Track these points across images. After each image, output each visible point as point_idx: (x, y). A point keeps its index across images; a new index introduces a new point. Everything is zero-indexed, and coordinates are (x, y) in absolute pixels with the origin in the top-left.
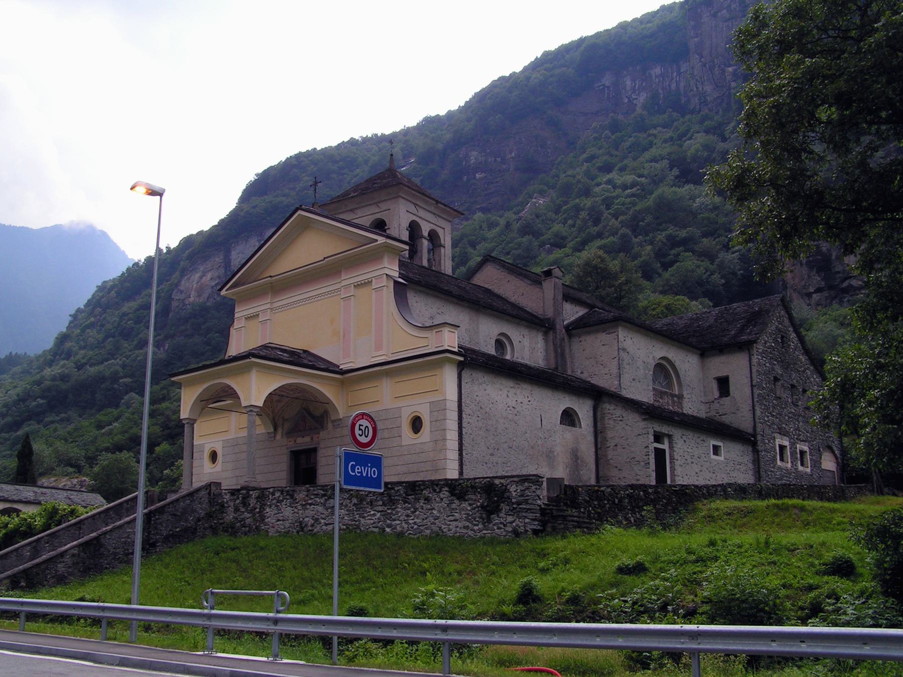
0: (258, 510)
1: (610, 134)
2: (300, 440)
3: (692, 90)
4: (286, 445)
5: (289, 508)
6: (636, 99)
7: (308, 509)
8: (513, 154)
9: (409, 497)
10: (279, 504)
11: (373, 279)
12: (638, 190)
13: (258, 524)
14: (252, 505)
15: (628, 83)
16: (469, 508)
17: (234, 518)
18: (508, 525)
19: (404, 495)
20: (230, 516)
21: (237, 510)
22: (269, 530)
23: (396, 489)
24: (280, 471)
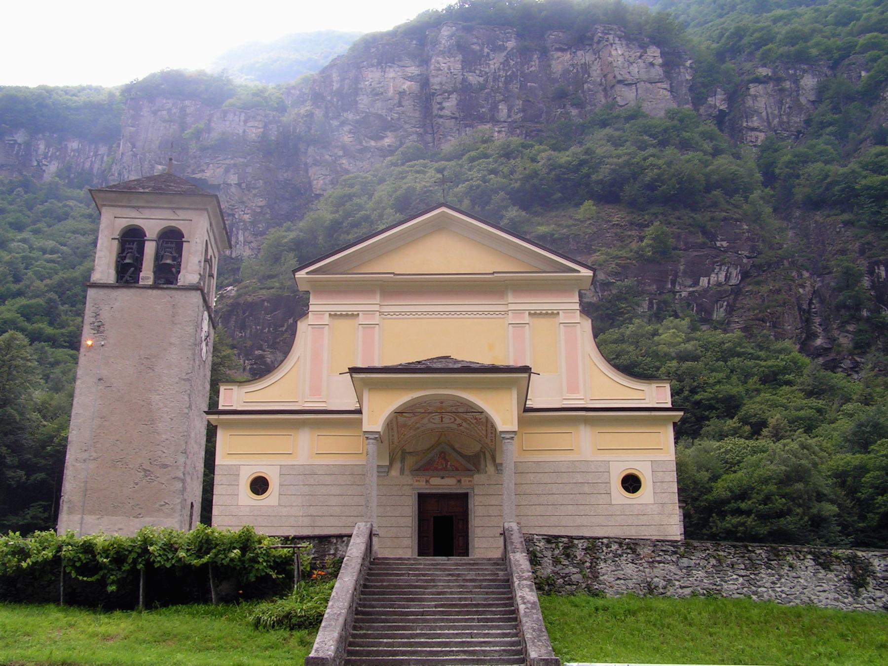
0: (588, 564)
2: (435, 481)
3: (113, 175)
4: (412, 485)
7: (656, 567)
9: (772, 562)
10: (617, 559)
11: (560, 312)
12: (59, 257)
13: (589, 582)
14: (579, 558)
15: (42, 147)
16: (836, 579)
17: (553, 572)
18: (878, 600)
19: (766, 560)
21: (556, 561)
22: (606, 591)
23: (758, 552)
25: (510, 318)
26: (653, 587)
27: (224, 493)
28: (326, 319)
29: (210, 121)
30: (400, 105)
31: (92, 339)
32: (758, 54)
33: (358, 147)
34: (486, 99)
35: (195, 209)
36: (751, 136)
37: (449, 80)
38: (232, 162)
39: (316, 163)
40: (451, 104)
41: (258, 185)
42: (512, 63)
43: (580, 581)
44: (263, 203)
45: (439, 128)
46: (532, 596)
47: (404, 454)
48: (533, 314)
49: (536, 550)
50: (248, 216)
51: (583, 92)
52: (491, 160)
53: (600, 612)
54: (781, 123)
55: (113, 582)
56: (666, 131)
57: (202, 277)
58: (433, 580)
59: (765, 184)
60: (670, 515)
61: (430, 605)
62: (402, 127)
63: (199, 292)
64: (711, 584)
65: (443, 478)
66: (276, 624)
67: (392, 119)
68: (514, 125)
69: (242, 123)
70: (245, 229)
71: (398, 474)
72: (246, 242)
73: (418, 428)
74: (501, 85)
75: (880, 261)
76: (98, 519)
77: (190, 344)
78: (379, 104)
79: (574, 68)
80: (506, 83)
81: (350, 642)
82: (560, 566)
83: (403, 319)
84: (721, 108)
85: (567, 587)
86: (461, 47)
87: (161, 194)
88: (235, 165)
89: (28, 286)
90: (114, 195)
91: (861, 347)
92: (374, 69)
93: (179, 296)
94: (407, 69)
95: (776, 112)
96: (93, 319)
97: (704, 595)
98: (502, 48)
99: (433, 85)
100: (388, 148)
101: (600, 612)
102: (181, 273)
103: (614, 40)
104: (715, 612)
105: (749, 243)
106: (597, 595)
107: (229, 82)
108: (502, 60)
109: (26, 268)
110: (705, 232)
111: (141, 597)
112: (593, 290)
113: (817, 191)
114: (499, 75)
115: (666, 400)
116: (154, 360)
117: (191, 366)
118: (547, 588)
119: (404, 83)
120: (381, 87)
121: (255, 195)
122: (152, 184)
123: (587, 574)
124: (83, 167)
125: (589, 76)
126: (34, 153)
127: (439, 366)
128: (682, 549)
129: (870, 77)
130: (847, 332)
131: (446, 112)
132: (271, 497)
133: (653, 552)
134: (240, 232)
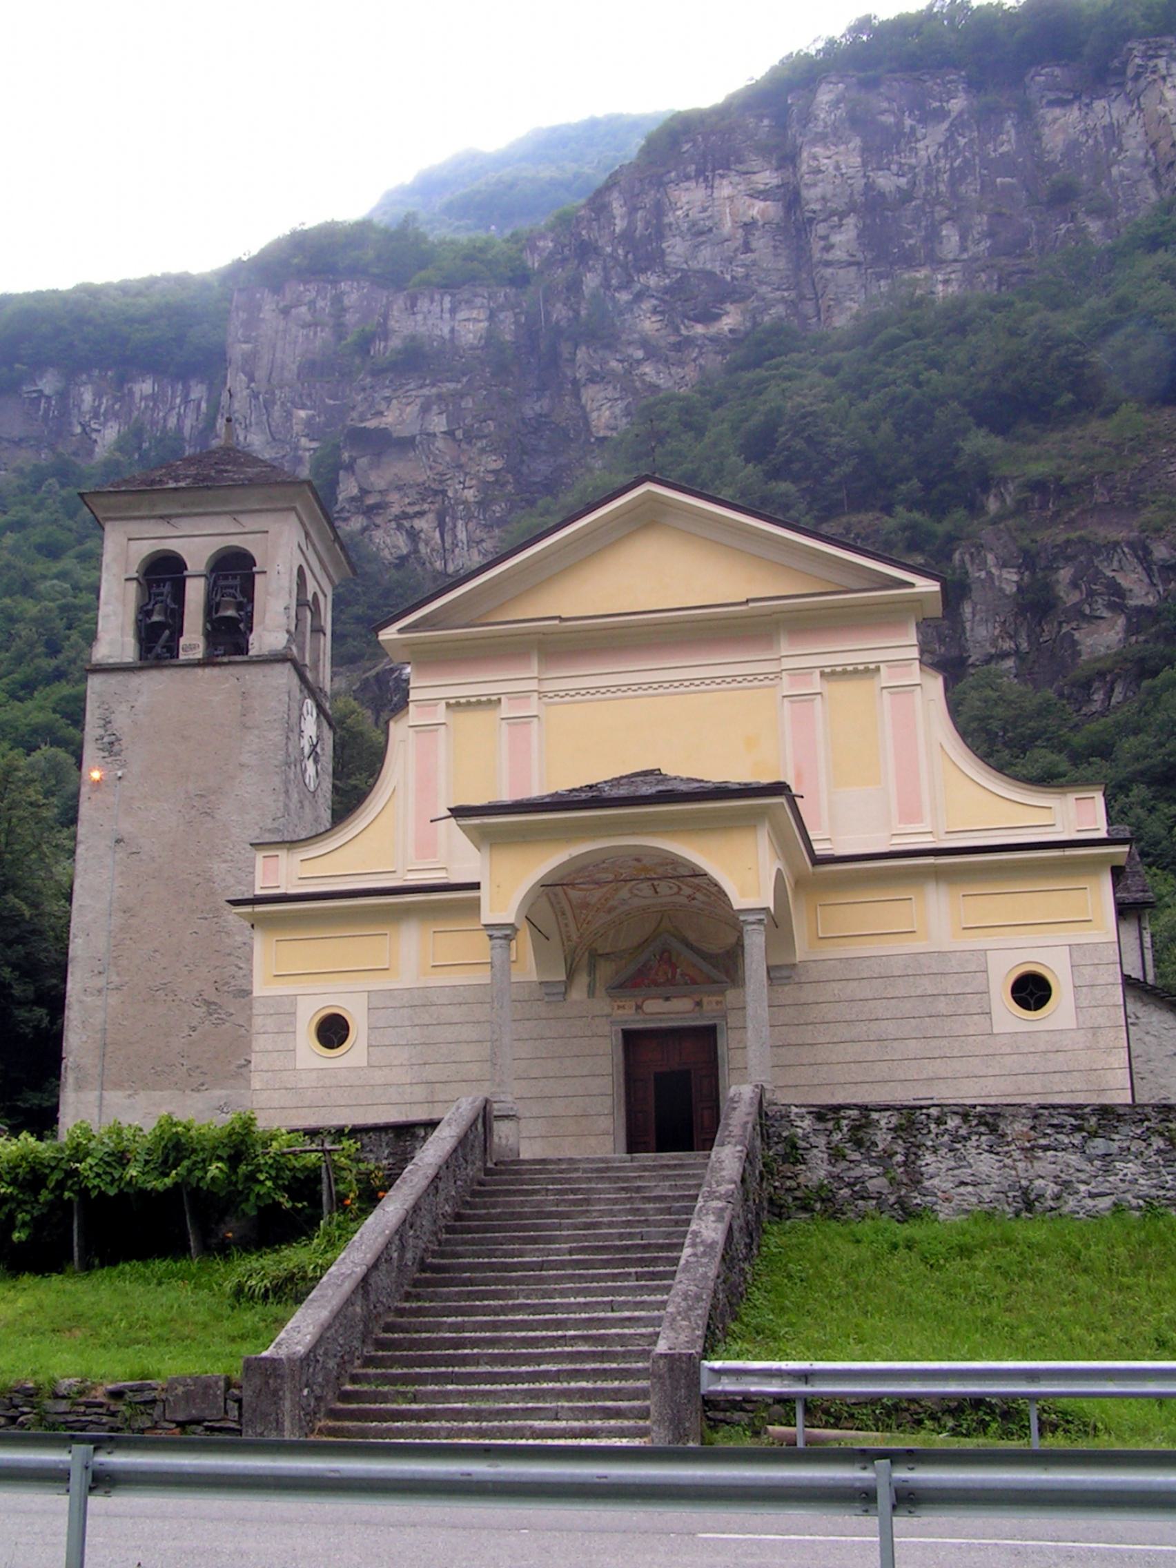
0: (899, 1158)
1: (57, 487)
2: (653, 1006)
4: (608, 1016)
5: (986, 1154)
6: (98, 431)
7: (1038, 1158)
10: (958, 1146)
11: (882, 666)
13: (903, 1192)
14: (881, 1146)
15: (88, 397)
17: (830, 1175)
20: (817, 1170)
21: (836, 1155)
22: (937, 1207)
24: (411, 1084)
25: (786, 686)
26: (1032, 1197)
27: (270, 1048)
28: (441, 714)
29: (386, 317)
30: (747, 248)
31: (100, 768)
33: (672, 339)
34: (915, 221)
35: (268, 510)
37: (838, 190)
38: (434, 390)
39: (594, 378)
40: (845, 238)
41: (486, 431)
42: (962, 141)
43: (885, 1191)
44: (499, 465)
45: (825, 287)
46: (715, 1230)
47: (595, 957)
48: (830, 675)
49: (796, 1135)
50: (472, 491)
51: (1110, 183)
52: (928, 340)
53: (902, 1251)
55: (24, 1224)
57: (295, 635)
58: (587, 1201)
60: (1109, 1050)
61: (560, 1251)
62: (754, 292)
63: (288, 665)
64: (1155, 1186)
65: (667, 999)
66: (271, 1293)
67: (733, 278)
68: (975, 266)
69: (447, 316)
70: (469, 518)
71: (585, 995)
72: (473, 542)
74: (942, 188)
76: (130, 1096)
77: (276, 763)
78: (706, 252)
79: (1089, 137)
80: (954, 183)
82: (844, 1164)
83: (605, 700)
85: (860, 1202)
86: (858, 121)
87: (208, 488)
88: (440, 397)
89: (72, 662)
90: (125, 498)
92: (692, 184)
93: (254, 677)
94: (755, 178)
96: (101, 732)
97: (1139, 1208)
98: (941, 114)
99: (807, 204)
100: (730, 336)
101: (902, 1251)
102: (254, 633)
104: (1146, 1244)
106: (919, 1216)
107: (420, 238)
108: (942, 139)
109: (69, 628)
111: (76, 1249)
112: (1147, 580)
114: (938, 170)
115: (1096, 823)
116: (213, 798)
117: (281, 805)
118: (818, 1206)
119: (750, 206)
120: (709, 218)
122: (192, 471)
123: (898, 1178)
124: (165, 427)
125: (1121, 149)
126: (76, 411)
127: (623, 791)
128: (1093, 1120)
131: (838, 254)
132: (354, 1052)
133: (1033, 1128)
134: (460, 523)
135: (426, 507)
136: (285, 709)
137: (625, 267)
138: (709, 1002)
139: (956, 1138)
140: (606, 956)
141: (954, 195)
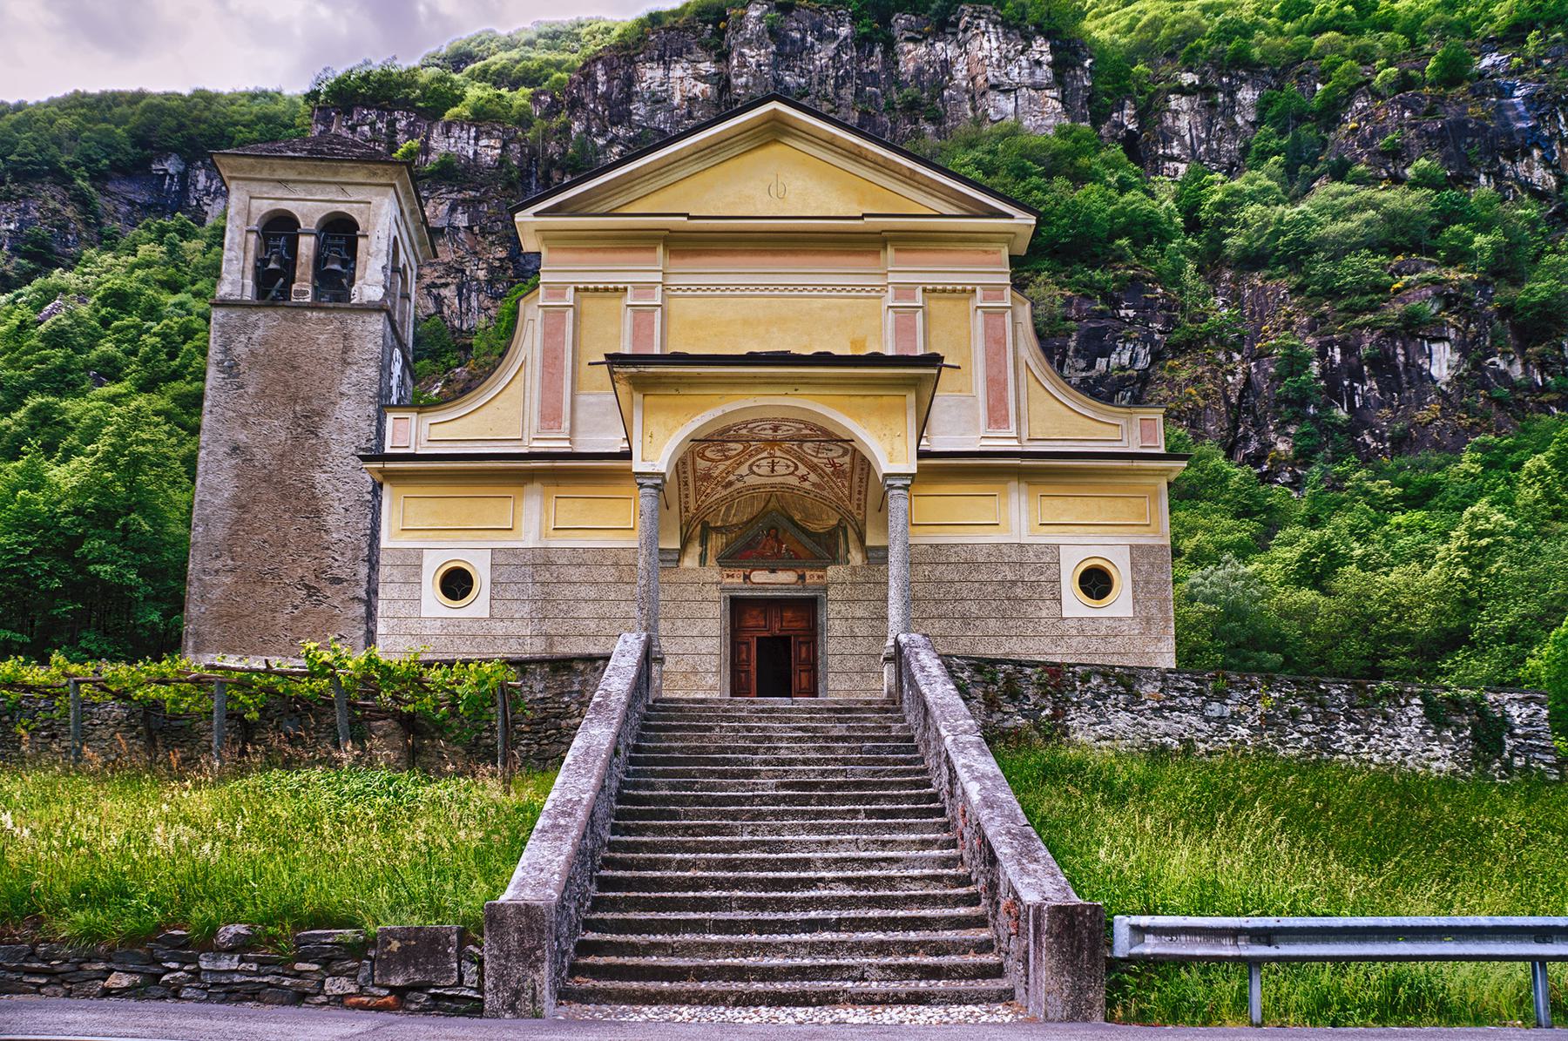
2: (759, 577)
4: (717, 583)
8: (12, 227)
10: (1100, 703)
11: (629, 286)
23: (1335, 692)
32: (1182, 53)
35: (370, 184)
36: (1168, 168)
42: (845, 58)
44: (504, 255)
47: (706, 532)
51: (942, 101)
54: (1209, 151)
56: (1055, 156)
59: (1187, 231)
61: (767, 785)
69: (472, 142)
70: (479, 291)
71: (696, 564)
73: (730, 484)
75: (1334, 340)
80: (837, 87)
81: (603, 859)
84: (1130, 127)
86: (775, 33)
88: (464, 201)
91: (1304, 456)
94: (700, 66)
95: (1203, 136)
96: (220, 357)
103: (987, 27)
105: (1164, 312)
110: (1107, 298)
113: (1255, 245)
121: (492, 243)
129: (1327, 92)
130: (1288, 435)
132: (477, 605)
135: (449, 280)
136: (380, 350)
137: (602, 119)
138: (812, 577)
139: (1098, 696)
140: (717, 530)
141: (837, 95)
